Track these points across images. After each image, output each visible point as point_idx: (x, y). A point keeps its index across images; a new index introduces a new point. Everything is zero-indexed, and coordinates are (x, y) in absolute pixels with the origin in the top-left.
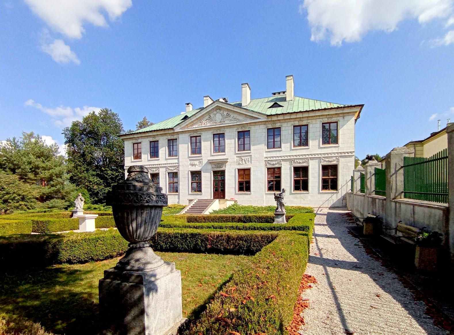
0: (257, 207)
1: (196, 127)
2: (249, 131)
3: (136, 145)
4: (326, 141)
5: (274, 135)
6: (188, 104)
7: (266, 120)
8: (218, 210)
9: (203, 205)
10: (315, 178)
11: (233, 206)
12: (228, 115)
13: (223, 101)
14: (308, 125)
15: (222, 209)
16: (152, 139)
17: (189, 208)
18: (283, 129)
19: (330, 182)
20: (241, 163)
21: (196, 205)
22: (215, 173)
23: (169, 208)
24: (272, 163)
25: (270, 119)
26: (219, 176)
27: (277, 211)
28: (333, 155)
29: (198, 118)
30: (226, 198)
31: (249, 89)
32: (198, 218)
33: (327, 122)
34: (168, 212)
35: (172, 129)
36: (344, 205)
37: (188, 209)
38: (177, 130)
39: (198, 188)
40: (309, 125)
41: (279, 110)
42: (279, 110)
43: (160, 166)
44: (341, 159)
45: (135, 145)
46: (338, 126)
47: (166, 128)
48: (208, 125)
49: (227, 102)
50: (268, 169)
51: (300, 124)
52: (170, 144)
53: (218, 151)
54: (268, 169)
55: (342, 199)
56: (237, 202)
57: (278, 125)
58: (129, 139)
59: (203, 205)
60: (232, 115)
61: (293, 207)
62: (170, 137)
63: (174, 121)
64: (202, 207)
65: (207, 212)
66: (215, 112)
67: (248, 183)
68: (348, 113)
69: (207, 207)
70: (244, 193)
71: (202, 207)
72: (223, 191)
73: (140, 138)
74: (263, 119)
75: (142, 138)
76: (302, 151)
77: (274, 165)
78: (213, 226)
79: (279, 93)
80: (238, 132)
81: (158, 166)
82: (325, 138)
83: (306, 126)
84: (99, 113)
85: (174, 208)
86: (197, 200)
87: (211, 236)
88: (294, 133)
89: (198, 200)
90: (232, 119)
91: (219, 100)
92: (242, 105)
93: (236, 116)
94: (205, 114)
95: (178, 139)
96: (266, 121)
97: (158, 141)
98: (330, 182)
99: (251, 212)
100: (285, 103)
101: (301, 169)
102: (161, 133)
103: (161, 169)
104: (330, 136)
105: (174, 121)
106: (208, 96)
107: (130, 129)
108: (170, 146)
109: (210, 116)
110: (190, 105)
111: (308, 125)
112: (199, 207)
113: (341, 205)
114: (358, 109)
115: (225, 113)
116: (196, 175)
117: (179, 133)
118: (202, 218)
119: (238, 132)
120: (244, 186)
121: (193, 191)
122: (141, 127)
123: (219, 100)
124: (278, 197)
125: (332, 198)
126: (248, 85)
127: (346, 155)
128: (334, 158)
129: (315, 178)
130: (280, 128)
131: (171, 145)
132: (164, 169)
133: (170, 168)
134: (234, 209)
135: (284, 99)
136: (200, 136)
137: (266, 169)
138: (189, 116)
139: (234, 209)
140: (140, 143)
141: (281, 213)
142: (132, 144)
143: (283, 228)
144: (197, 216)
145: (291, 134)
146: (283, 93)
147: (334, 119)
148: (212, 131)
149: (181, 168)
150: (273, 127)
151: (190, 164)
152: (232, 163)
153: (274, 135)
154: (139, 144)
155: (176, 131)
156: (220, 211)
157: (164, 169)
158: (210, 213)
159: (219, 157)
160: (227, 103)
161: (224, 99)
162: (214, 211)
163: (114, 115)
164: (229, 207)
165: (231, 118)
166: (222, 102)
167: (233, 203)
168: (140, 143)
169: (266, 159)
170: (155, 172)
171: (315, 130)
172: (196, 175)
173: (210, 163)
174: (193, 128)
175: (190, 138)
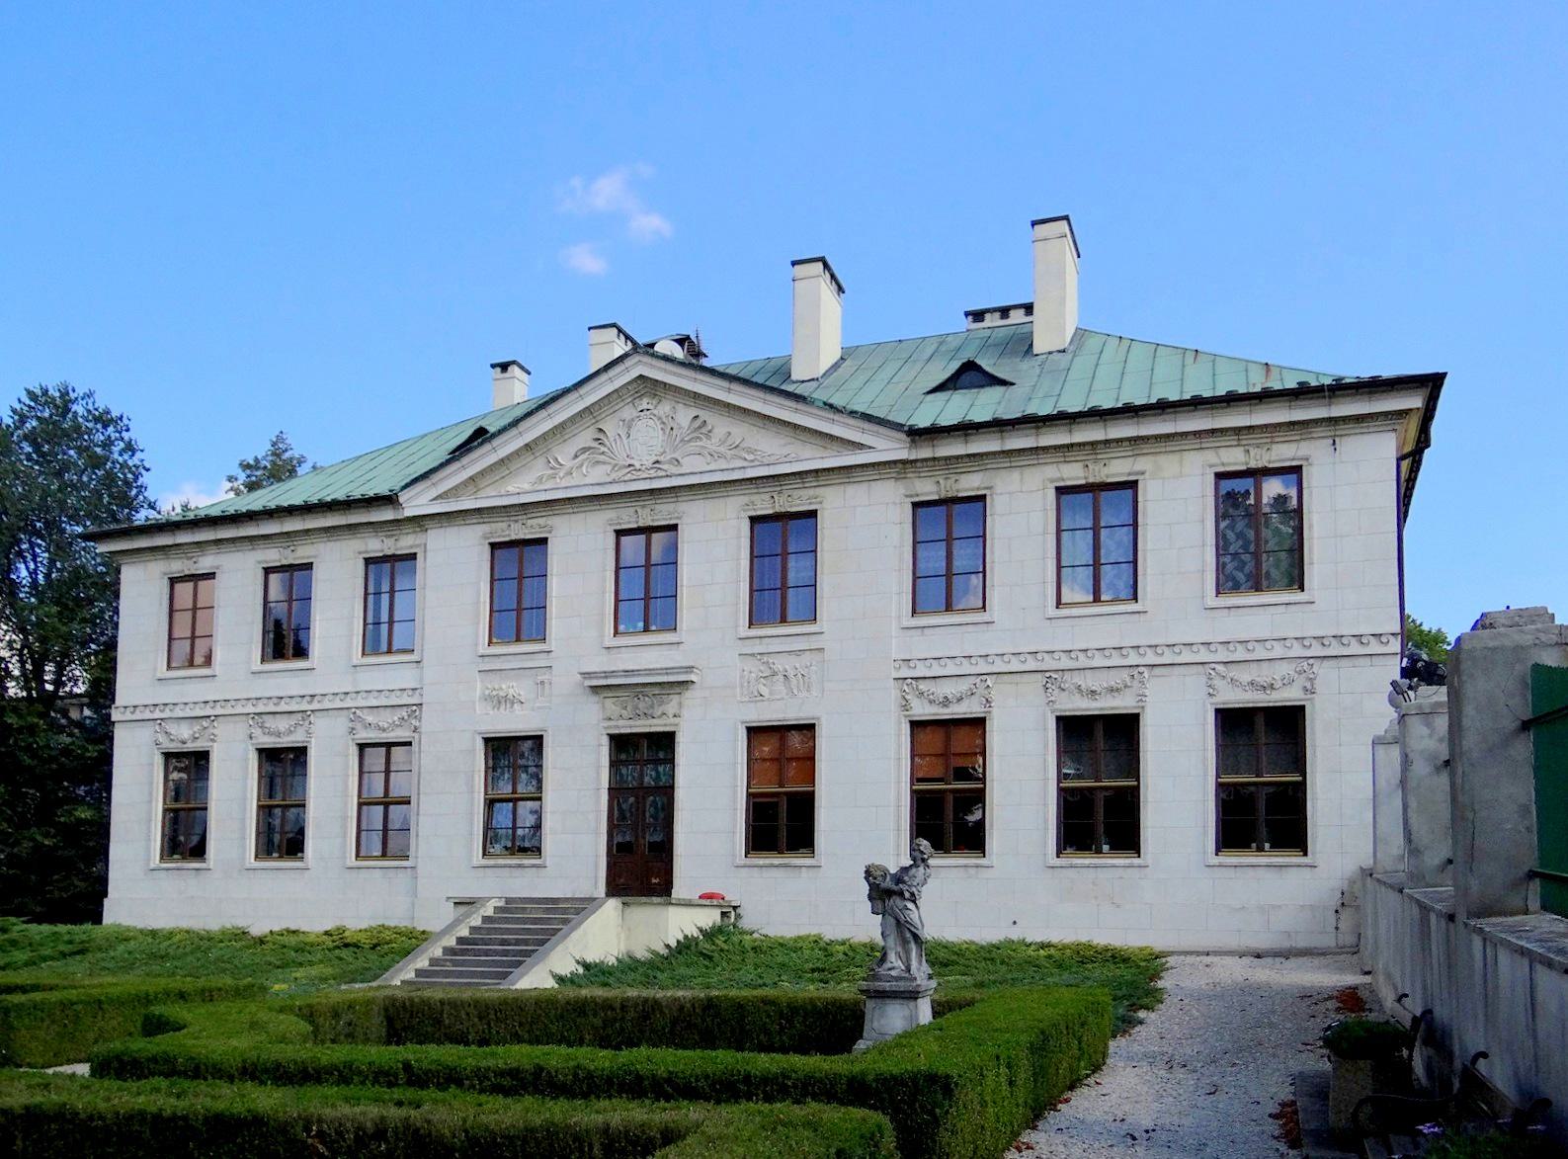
0: (843, 943)
1: (522, 486)
2: (813, 514)
3: (184, 590)
4: (1241, 577)
5: (949, 540)
6: (504, 367)
7: (903, 455)
8: (612, 961)
9: (537, 924)
10: (1179, 779)
11: (710, 934)
12: (700, 428)
13: (678, 353)
14: (1136, 482)
15: (641, 954)
16: (274, 556)
17: (448, 951)
18: (996, 507)
19: (1262, 808)
20: (765, 691)
21: (489, 931)
22: (621, 744)
23: (346, 945)
24: (948, 689)
25: (925, 453)
26: (643, 766)
27: (882, 971)
28: (1278, 651)
29: (535, 441)
30: (679, 891)
31: (834, 287)
32: (446, 1008)
33: (635, 526)
34: (329, 971)
35: (389, 500)
36: (1348, 939)
37: (438, 953)
38: (417, 503)
39: (513, 837)
40: (1140, 486)
41: (982, 405)
42: (982, 405)
43: (315, 706)
44: (1323, 670)
45: (178, 587)
46: (1305, 492)
47: (357, 494)
48: (592, 478)
49: (698, 354)
50: (916, 725)
51: (1253, 465)
52: (378, 584)
53: (641, 625)
54: (916, 725)
55: (1335, 901)
56: (738, 917)
57: (969, 483)
58: (148, 556)
59: (537, 924)
60: (720, 425)
61: (1049, 945)
62: (377, 545)
63: (414, 458)
64: (517, 942)
65: (536, 979)
66: (628, 412)
67: (802, 808)
68: (1359, 419)
69: (542, 943)
70: (776, 861)
71: (517, 942)
72: (664, 851)
73: (213, 549)
74: (889, 448)
75: (224, 548)
76: (1102, 630)
77: (946, 702)
78: (407, 1066)
79: (1004, 312)
80: (754, 520)
81: (305, 706)
82: (1235, 555)
83: (1129, 493)
84: (18, 406)
85: (374, 947)
86: (501, 904)
87: (321, 1135)
88: (1059, 531)
89: (508, 900)
90: (722, 449)
91: (652, 345)
92: (794, 377)
93: (740, 430)
94: (572, 420)
95: (420, 557)
96: (904, 462)
97: (309, 566)
98: (1262, 808)
99: (798, 975)
100: (1026, 365)
101: (1099, 731)
102: (328, 525)
103: (1000, 692)
104: (1261, 545)
105: (414, 458)
106: (614, 325)
107: (184, 500)
108: (378, 594)
109: (601, 430)
110: (515, 370)
111: (1136, 482)
112: (504, 942)
113: (1328, 941)
114: (1415, 401)
115: (684, 415)
116: (513, 757)
117: (428, 524)
118: (471, 1010)
119: (754, 520)
120: (781, 822)
121: (498, 848)
122: (252, 487)
123: (652, 345)
124: (889, 893)
125: (1275, 894)
126: (826, 266)
127: (1337, 649)
128: (1285, 669)
129: (1179, 779)
130: (983, 498)
131: (385, 587)
132: (1195, 681)
133: (370, 719)
134: (710, 958)
135: (1023, 345)
136: (674, 528)
137: (906, 729)
138: (492, 429)
139: (710, 958)
140: (211, 576)
141: (902, 986)
142: (166, 583)
143: (795, 1086)
144: (442, 1002)
145: (1045, 533)
146: (975, 321)
147: (1282, 453)
148: (745, 499)
149: (429, 722)
150: (943, 495)
151: (486, 698)
152: (720, 685)
153: (949, 540)
154: (202, 584)
155: (408, 513)
156: (630, 966)
157: (341, 723)
158: (560, 979)
159: (647, 656)
160: (704, 362)
161: (681, 341)
162: (587, 966)
163: (104, 420)
164: (685, 946)
165: (712, 444)
166: (666, 358)
167: (709, 918)
168: (211, 576)
169: (905, 673)
170: (285, 741)
171: (1178, 504)
172: (513, 757)
173: (595, 689)
174: (509, 495)
175: (612, 538)
